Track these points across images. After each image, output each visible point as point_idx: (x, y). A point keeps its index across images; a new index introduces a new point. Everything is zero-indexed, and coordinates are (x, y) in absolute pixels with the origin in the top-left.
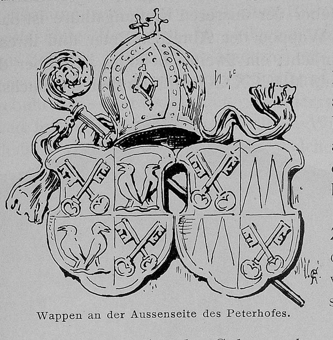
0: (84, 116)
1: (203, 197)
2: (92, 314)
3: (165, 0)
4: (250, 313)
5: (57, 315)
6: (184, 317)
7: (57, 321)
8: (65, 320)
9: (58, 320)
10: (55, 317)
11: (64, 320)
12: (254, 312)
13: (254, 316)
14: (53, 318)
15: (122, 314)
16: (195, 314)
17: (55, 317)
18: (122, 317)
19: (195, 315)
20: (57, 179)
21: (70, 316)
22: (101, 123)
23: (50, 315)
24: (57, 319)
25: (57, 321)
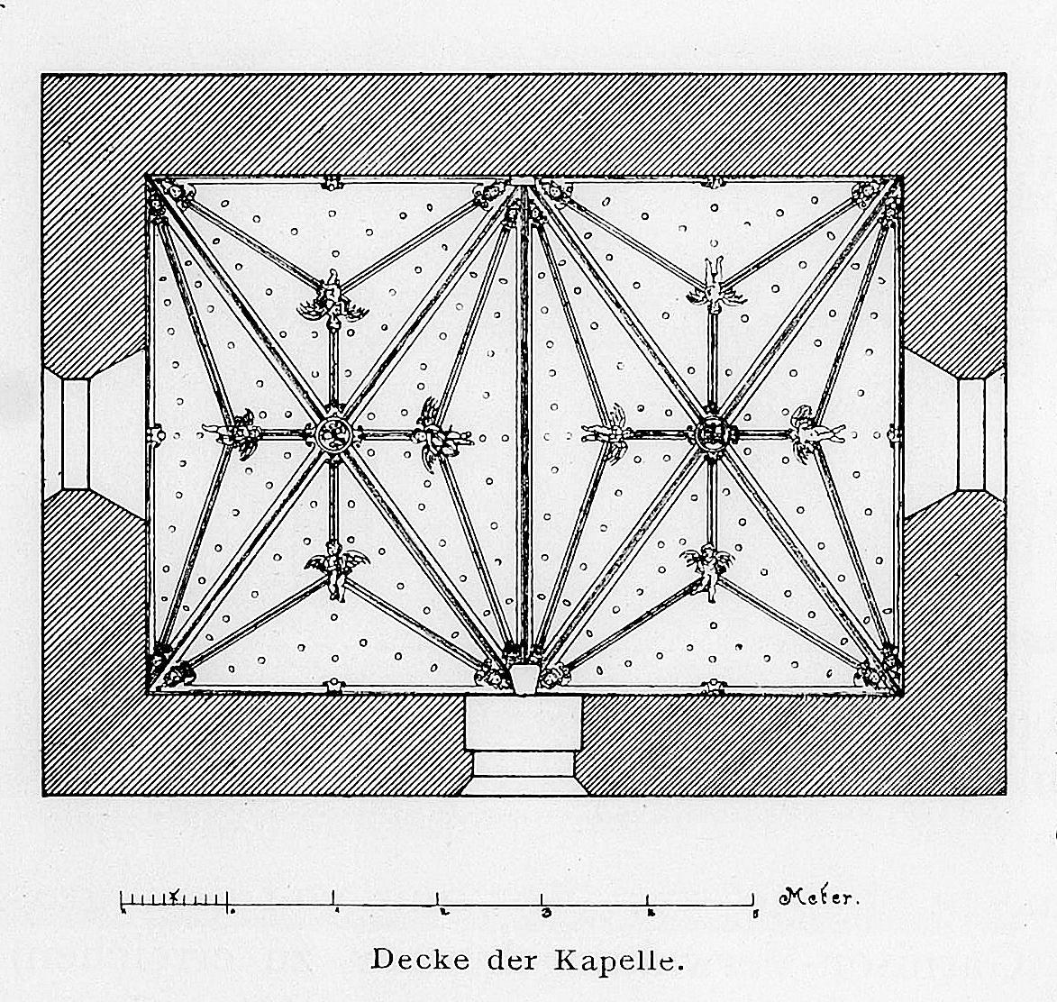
0: (717, 366)
1: (338, 459)
2: (592, 959)
3: (896, 1)
4: (463, 958)
5: (603, 959)
6: (641, 968)
7: (604, 976)
8: (607, 973)
9: (606, 972)
10: (598, 963)
11: (603, 973)
12: (529, 957)
13: (529, 967)
14: (592, 968)
15: (530, 959)
16: (466, 960)
17: (598, 963)
18: (529, 967)
19: (466, 963)
20: (701, 584)
21: (622, 961)
22: (185, 73)
23: (584, 958)
24: (604, 969)
25: (604, 976)
